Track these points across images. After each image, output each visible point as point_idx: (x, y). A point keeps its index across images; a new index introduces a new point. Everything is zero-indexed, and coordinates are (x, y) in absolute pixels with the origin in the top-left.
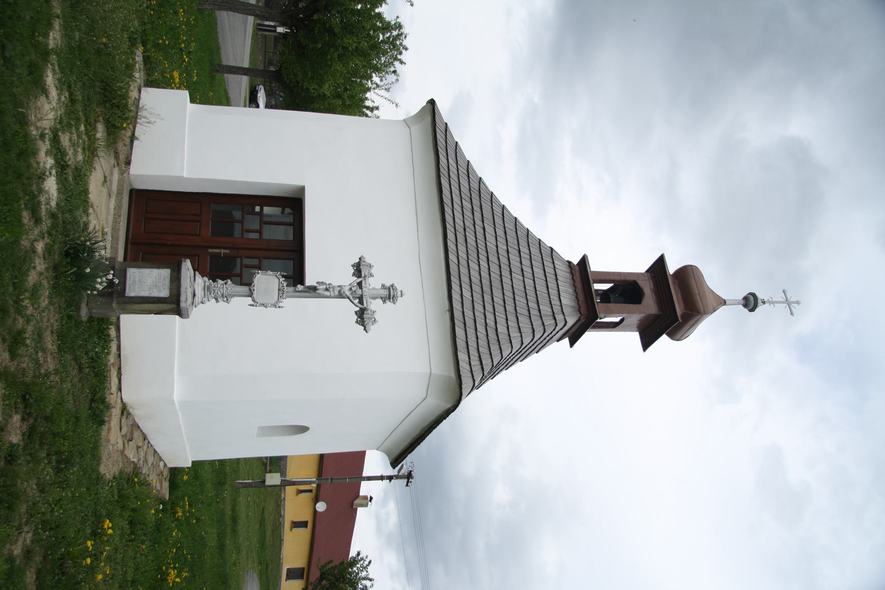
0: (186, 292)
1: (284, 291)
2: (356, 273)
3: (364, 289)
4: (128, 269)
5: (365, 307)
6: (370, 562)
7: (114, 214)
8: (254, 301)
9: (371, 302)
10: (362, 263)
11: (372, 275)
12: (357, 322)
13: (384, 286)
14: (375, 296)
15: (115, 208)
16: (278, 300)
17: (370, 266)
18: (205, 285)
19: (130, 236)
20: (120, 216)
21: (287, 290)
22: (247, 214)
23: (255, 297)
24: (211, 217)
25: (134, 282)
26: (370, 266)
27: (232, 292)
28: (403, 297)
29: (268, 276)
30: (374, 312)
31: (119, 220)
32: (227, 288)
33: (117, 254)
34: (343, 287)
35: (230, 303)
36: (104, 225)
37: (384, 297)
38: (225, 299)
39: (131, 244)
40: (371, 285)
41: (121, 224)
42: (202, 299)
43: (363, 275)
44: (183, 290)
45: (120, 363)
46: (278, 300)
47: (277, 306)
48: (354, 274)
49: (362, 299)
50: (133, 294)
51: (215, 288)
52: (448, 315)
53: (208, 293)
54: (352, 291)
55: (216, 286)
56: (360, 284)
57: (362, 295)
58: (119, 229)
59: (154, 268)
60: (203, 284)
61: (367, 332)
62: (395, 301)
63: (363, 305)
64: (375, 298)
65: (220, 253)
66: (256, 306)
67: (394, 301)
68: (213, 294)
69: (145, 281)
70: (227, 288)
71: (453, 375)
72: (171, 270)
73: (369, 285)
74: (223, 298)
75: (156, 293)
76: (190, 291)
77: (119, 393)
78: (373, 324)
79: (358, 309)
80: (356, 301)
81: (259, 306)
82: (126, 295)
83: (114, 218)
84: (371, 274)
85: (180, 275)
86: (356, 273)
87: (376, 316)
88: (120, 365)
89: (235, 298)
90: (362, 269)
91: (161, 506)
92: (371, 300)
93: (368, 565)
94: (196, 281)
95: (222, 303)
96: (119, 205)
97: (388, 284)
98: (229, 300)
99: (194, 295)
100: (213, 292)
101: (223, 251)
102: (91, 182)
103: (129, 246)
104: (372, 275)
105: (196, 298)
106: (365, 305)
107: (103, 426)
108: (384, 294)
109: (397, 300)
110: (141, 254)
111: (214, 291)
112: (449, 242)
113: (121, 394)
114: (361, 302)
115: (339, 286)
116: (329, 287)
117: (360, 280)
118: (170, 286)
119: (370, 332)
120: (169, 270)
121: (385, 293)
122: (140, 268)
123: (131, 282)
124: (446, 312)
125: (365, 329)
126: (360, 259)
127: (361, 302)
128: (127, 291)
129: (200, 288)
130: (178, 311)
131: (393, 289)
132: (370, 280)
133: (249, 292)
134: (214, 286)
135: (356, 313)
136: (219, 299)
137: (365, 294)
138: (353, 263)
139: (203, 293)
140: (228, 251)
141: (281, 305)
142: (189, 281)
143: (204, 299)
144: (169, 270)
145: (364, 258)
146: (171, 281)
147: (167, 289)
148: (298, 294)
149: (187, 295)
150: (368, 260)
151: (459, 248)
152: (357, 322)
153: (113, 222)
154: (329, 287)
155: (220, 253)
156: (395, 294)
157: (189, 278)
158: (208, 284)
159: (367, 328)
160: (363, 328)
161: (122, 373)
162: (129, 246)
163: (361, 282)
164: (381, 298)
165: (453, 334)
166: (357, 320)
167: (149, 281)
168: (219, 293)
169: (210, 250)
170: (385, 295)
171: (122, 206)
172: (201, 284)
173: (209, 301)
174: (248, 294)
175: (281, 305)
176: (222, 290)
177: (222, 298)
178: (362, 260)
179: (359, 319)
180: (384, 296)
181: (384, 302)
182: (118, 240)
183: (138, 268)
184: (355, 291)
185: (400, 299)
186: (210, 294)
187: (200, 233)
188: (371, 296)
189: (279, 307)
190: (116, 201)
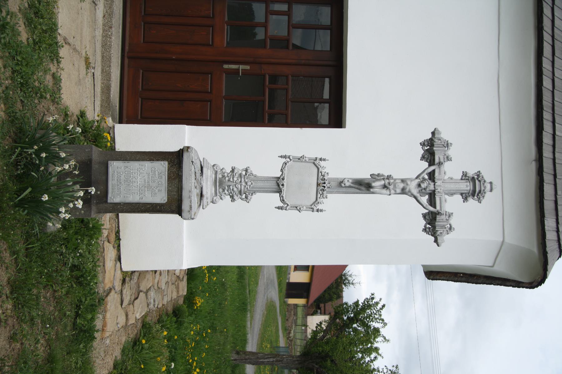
0: (190, 197)
1: (324, 187)
2: (426, 156)
3: (438, 183)
4: (109, 162)
5: (437, 211)
6: (384, 306)
7: (104, 25)
8: (283, 201)
9: (445, 201)
10: (437, 142)
11: (448, 159)
12: (425, 230)
13: (466, 176)
14: (452, 192)
15: (104, 16)
16: (317, 199)
17: (447, 144)
18: (216, 178)
19: (127, 48)
20: (111, 27)
21: (328, 185)
22: (271, 14)
23: (284, 196)
24: (226, 19)
25: (119, 180)
26: (447, 145)
27: (253, 188)
28: (494, 191)
29: (303, 164)
30: (449, 216)
31: (110, 33)
32: (246, 183)
33: (110, 81)
34: (409, 182)
35: (250, 202)
36: (88, 53)
37: (465, 193)
38: (244, 196)
39: (129, 58)
40: (447, 173)
41: (113, 38)
42: (213, 199)
43: (437, 161)
44: (185, 194)
45: (118, 225)
46: (317, 199)
47: (315, 209)
48: (423, 158)
49: (435, 198)
50: (117, 200)
51: (229, 183)
52: (533, 167)
53: (221, 190)
54: (420, 189)
55: (231, 180)
56: (432, 176)
57: (434, 191)
58: (110, 46)
59: (146, 160)
60: (214, 176)
61: (438, 245)
62: (481, 198)
63: (435, 207)
64: (451, 194)
65: (238, 69)
66: (286, 210)
67: (479, 199)
68: (228, 191)
69: (134, 180)
70: (246, 183)
71: (535, 249)
72: (169, 164)
73: (445, 173)
74: (241, 195)
75: (149, 198)
76: (196, 192)
77: (118, 263)
78: (448, 234)
79: (426, 211)
80: (424, 199)
81: (289, 209)
82: (109, 201)
83: (104, 30)
84: (447, 157)
85: (182, 172)
86: (426, 156)
87: (453, 221)
88: (118, 227)
89: (258, 194)
90: (436, 152)
91: (173, 364)
92: (447, 197)
93: (381, 309)
94: (204, 175)
95: (239, 202)
96: (108, 11)
97: (471, 173)
98: (249, 198)
99: (202, 195)
100: (227, 188)
101: (242, 67)
102: (60, 10)
103: (126, 61)
104: (448, 159)
105: (205, 199)
106: (438, 207)
107: (94, 342)
108: (466, 189)
109: (483, 197)
110: (141, 71)
111: (229, 186)
112: (544, 60)
113: (121, 264)
114: (432, 201)
115: (403, 181)
116: (389, 183)
117: (432, 168)
118: (169, 186)
119: (443, 245)
120: (166, 163)
121: (466, 187)
122: (126, 160)
123: (115, 182)
124: (531, 163)
125: (436, 241)
126: (433, 133)
127: (432, 201)
128: (110, 195)
129: (209, 183)
130: (179, 211)
131: (480, 181)
132: (447, 166)
133: (277, 187)
134: (229, 181)
135: (424, 216)
136: (235, 197)
137: (439, 190)
138: (422, 140)
139: (213, 189)
140: (248, 67)
141: (320, 207)
142: (193, 181)
143: (215, 198)
144: (166, 163)
145: (439, 133)
146: (170, 179)
147: (163, 190)
148: (344, 190)
149: (191, 201)
150: (445, 135)
151: (556, 65)
152: (425, 230)
153: (103, 37)
154: (389, 183)
155: (238, 69)
156: (482, 188)
157: (193, 175)
158: (220, 176)
159: (439, 241)
160: (433, 238)
161: (121, 238)
162: (126, 61)
163: (434, 171)
164: (462, 194)
165: (540, 196)
166: (425, 226)
167: (139, 180)
168: (235, 189)
169: (226, 66)
170: (467, 190)
171: (112, 12)
172: (211, 176)
173: (221, 199)
174: (274, 190)
175: (320, 207)
176: (239, 186)
177: (239, 196)
178: (436, 136)
179: (428, 226)
180: (466, 192)
181: (465, 199)
182: (110, 62)
183: (123, 160)
184: (425, 189)
185: (488, 195)
186: (224, 190)
187: (212, 43)
188: (447, 192)
189: (318, 211)
190: (105, 7)
